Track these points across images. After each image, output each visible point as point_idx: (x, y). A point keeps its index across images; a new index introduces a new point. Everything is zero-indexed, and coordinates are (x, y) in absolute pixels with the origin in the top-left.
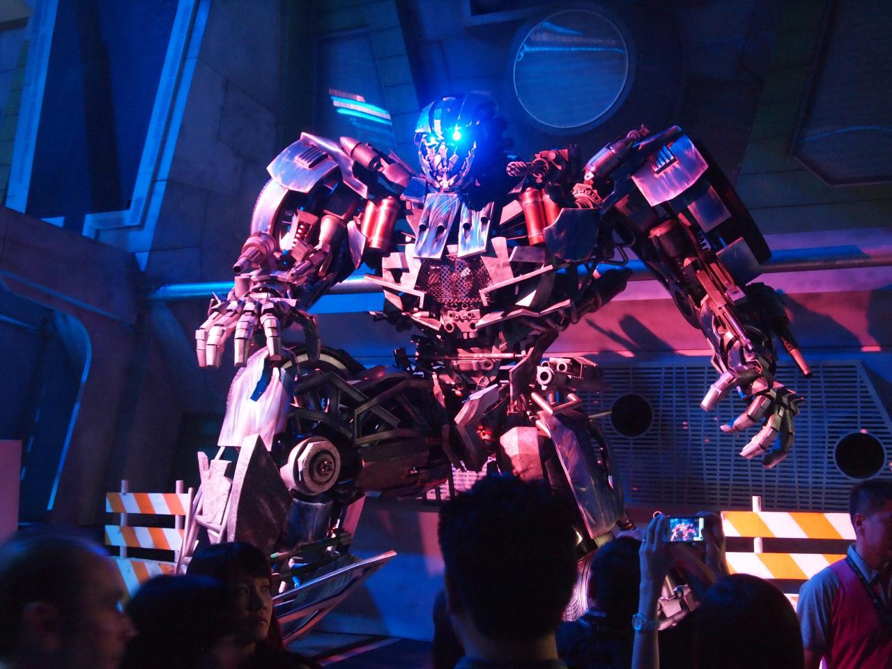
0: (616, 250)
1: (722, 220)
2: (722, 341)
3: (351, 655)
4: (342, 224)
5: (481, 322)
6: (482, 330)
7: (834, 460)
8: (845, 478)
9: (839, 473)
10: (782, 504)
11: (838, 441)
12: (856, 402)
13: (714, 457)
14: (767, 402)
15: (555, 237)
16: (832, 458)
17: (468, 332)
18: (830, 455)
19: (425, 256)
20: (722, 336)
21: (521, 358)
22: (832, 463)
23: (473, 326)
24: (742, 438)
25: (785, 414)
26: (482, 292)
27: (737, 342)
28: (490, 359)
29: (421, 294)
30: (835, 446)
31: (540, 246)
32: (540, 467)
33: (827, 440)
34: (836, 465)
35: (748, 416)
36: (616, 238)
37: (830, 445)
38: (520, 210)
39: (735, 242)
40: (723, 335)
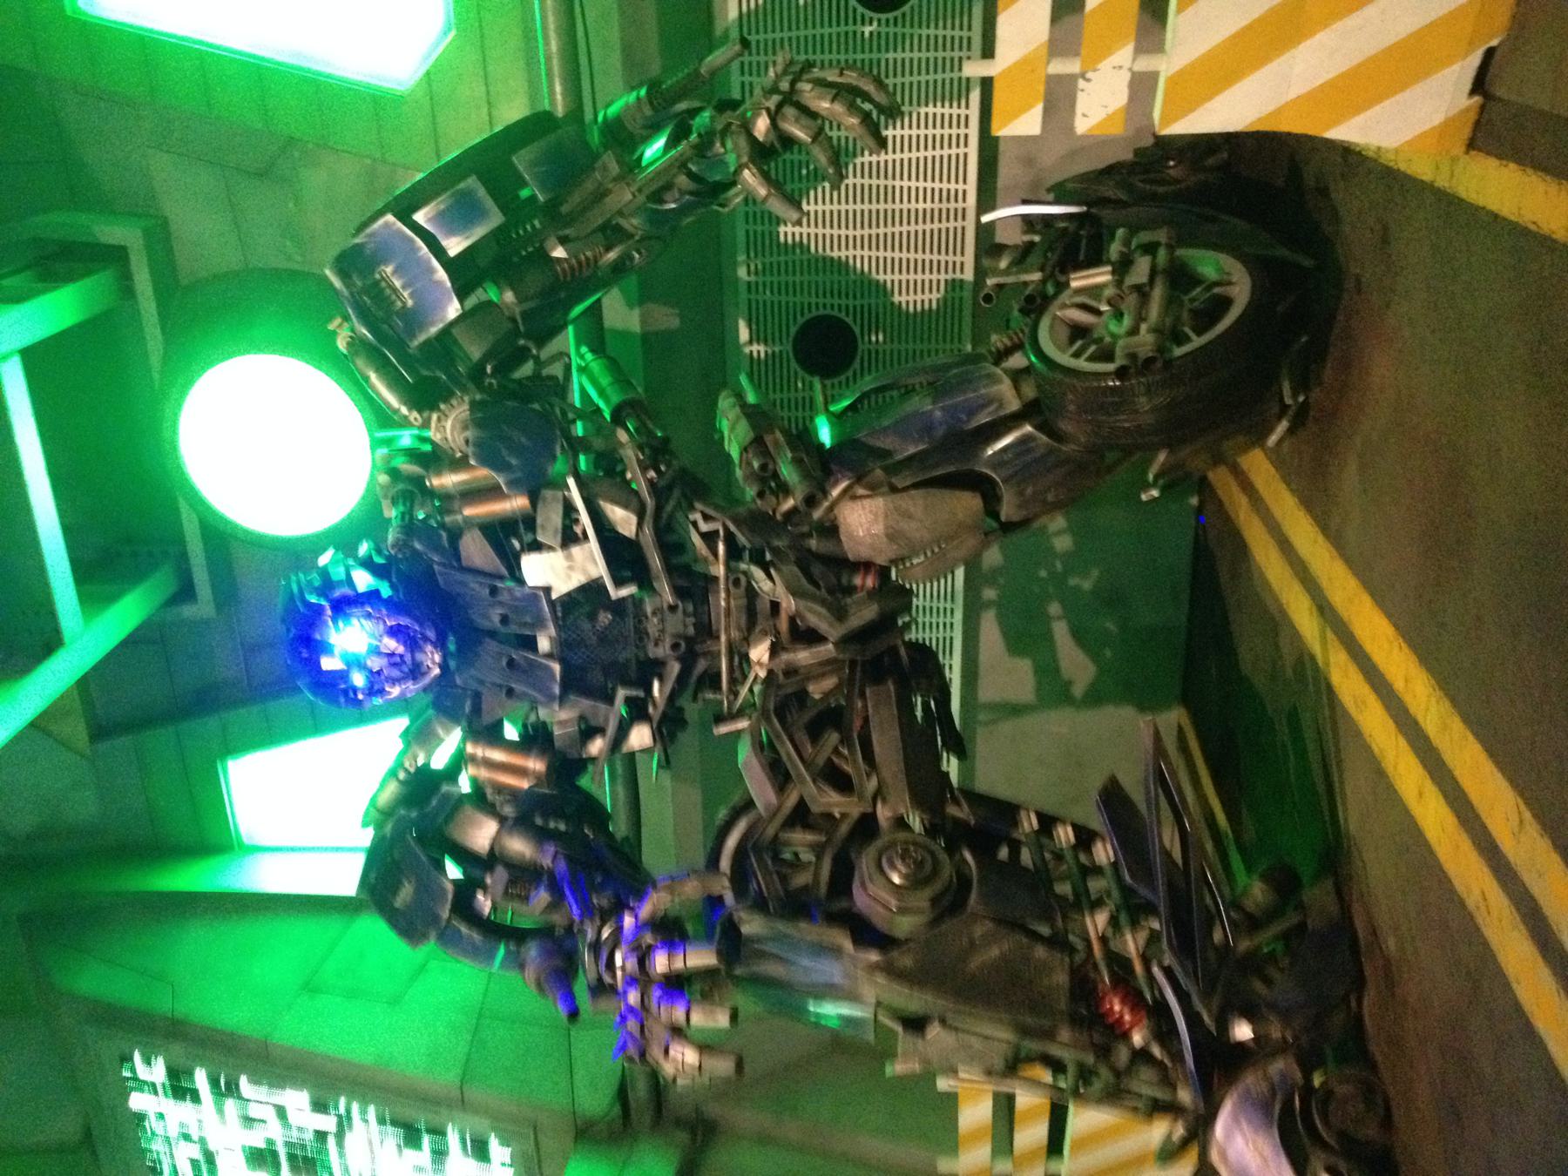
0: (545, 372)
1: (482, 192)
2: (691, 193)
3: (1232, 842)
4: (510, 822)
5: (668, 597)
6: (679, 592)
7: (891, 15)
8: (788, 335)
9: (912, 7)
10: (752, 239)
11: (849, 320)
12: (822, 52)
13: (889, 213)
14: (790, 111)
15: (519, 474)
16: (888, 21)
17: (679, 624)
18: (883, 22)
19: (557, 690)
20: (682, 193)
21: (726, 529)
22: (896, 19)
23: (673, 608)
24: (859, 18)
25: (809, 81)
26: (616, 593)
27: (690, 166)
28: (727, 579)
29: (621, 693)
30: (842, 315)
31: (534, 499)
32: (904, 494)
33: (851, 302)
34: (898, 13)
35: (813, 142)
36: (527, 369)
37: (843, 308)
38: (477, 533)
39: (521, 168)
40: (680, 190)
